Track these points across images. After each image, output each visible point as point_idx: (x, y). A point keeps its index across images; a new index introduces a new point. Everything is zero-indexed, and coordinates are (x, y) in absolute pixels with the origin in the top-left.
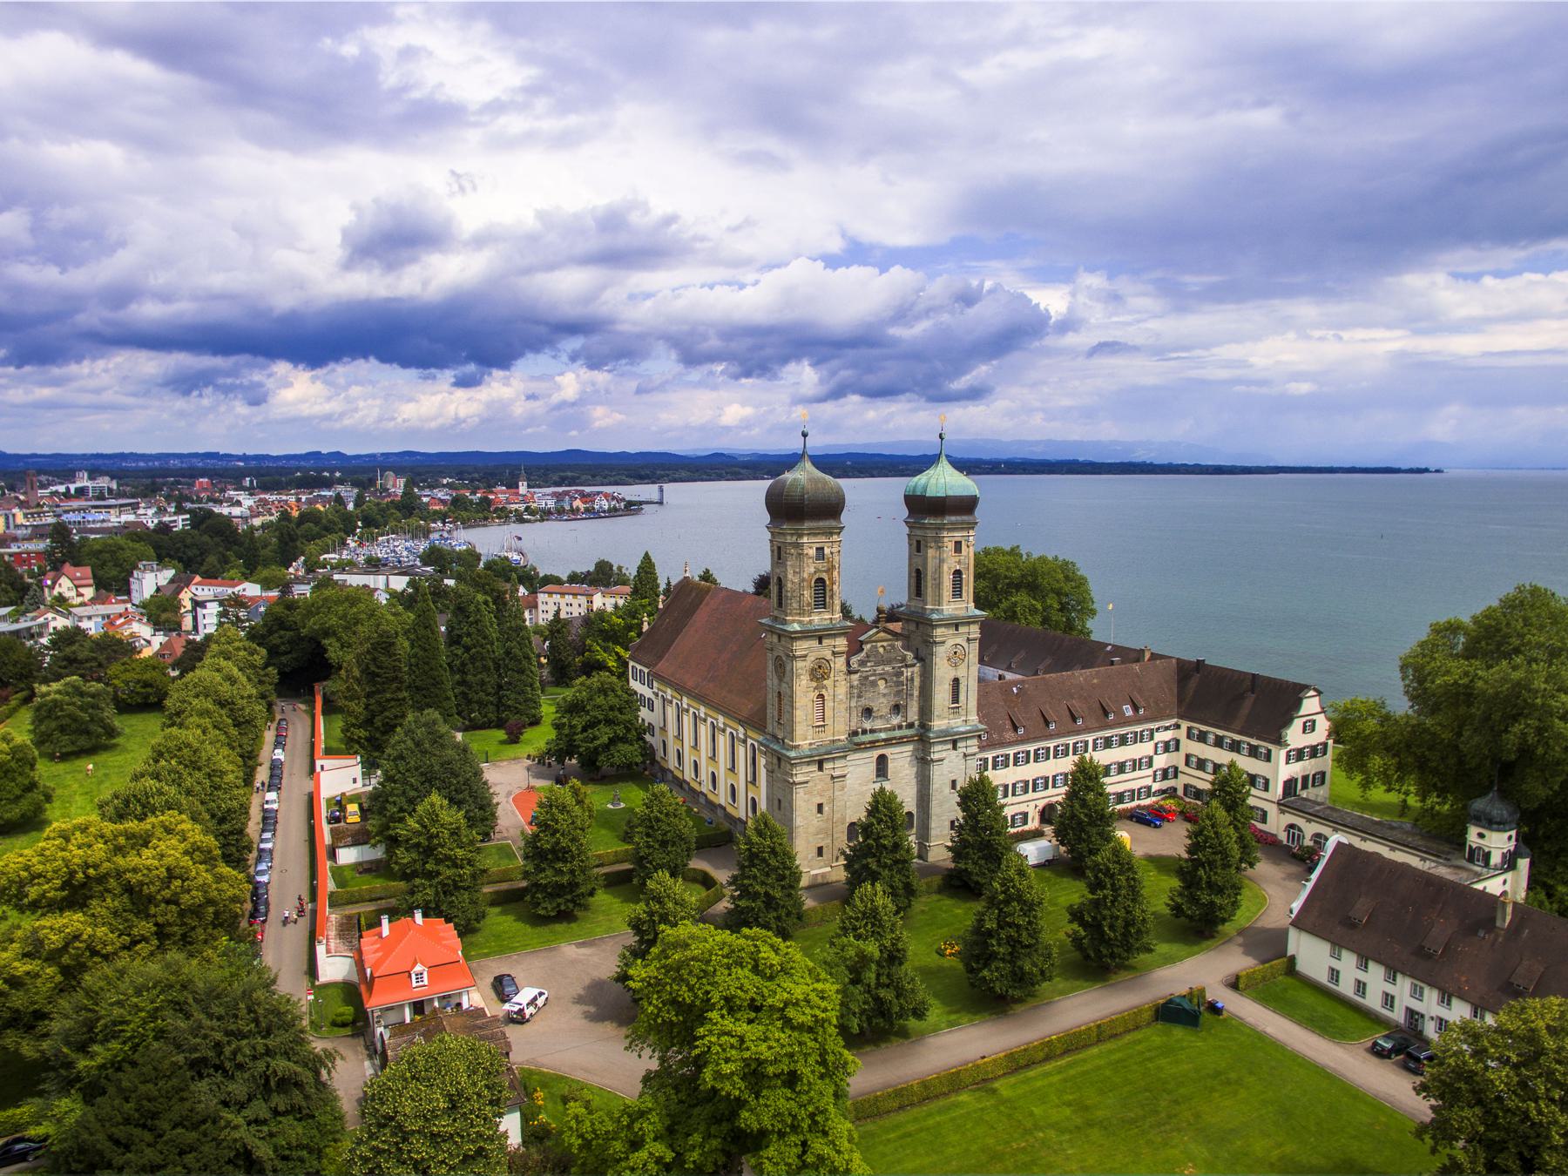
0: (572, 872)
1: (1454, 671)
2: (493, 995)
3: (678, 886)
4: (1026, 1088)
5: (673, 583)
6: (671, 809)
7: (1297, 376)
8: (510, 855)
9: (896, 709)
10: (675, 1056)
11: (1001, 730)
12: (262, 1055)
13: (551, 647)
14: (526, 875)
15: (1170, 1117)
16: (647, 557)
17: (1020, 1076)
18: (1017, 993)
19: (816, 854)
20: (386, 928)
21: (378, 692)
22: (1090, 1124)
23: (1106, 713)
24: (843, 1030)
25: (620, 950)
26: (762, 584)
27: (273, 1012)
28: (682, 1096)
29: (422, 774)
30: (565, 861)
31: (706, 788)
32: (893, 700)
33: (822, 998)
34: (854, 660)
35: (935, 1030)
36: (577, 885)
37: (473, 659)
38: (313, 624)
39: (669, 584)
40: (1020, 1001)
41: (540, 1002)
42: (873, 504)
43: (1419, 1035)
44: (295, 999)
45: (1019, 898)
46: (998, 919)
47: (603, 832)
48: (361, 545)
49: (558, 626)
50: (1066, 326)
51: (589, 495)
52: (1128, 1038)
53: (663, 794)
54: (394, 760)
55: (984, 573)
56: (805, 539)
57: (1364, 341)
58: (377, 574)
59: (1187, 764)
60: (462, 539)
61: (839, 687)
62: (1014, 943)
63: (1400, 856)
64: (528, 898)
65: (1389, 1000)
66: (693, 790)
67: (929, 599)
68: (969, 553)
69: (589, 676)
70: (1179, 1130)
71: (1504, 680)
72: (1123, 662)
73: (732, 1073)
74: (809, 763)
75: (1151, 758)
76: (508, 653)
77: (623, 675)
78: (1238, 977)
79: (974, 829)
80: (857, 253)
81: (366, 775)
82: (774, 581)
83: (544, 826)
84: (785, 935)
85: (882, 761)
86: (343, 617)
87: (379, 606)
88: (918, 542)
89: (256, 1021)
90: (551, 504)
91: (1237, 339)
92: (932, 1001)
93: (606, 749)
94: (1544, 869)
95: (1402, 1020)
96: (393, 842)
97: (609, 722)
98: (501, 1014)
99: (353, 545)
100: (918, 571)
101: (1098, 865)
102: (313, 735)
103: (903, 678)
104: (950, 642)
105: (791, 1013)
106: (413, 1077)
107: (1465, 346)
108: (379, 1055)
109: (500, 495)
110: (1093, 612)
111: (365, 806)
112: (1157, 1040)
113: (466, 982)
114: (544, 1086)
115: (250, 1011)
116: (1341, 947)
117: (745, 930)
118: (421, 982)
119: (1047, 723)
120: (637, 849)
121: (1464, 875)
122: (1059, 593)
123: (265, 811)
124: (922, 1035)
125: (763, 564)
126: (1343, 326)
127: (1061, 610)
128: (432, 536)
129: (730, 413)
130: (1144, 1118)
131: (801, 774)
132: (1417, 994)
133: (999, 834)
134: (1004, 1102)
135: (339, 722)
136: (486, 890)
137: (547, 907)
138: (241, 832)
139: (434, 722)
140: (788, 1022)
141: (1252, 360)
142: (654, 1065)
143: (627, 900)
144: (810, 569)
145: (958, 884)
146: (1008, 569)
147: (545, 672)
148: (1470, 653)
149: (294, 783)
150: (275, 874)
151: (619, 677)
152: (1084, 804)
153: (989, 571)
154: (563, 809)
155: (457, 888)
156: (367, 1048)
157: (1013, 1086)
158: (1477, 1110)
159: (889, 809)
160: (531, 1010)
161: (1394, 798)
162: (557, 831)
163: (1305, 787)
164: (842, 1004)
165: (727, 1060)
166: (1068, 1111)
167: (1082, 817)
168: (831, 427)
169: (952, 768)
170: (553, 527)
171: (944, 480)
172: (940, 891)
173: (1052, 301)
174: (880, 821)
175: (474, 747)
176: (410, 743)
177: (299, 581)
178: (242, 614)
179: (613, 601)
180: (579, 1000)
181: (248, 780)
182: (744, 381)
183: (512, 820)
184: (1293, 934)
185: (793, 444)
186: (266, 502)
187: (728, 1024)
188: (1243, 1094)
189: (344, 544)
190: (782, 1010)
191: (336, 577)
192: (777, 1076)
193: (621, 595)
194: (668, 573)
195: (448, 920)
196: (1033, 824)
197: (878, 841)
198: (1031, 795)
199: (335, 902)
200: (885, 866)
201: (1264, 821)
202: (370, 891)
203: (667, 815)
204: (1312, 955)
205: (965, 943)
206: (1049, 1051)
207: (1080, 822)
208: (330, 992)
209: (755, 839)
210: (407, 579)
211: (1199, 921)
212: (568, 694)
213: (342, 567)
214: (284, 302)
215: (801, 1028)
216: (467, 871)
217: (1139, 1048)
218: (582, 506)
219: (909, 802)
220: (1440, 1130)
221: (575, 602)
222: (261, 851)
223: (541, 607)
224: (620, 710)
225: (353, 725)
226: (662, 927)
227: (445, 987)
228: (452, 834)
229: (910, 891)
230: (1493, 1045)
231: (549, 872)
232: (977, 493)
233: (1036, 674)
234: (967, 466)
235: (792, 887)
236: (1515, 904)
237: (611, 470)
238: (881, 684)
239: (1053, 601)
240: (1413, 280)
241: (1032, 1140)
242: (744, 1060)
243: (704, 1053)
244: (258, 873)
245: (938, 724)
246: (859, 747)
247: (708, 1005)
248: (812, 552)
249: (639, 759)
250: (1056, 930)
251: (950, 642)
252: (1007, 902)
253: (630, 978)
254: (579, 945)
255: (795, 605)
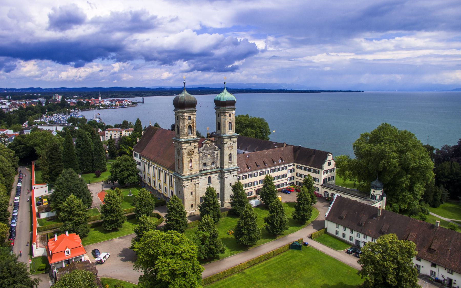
0: (116, 216)
1: (366, 147)
2: (92, 256)
3: (149, 219)
4: (254, 271)
5: (147, 127)
6: (147, 195)
7: (326, 65)
8: (97, 212)
9: (213, 163)
10: (149, 270)
11: (244, 168)
12: (12, 284)
13: (109, 147)
14: (102, 218)
15: (294, 276)
16: (138, 119)
17: (252, 268)
18: (250, 244)
19: (191, 206)
20: (56, 238)
21: (53, 163)
22: (272, 280)
23: (274, 162)
24: (199, 259)
25: (132, 239)
26: (173, 127)
27: (16, 269)
28: (151, 282)
29: (68, 188)
30: (114, 213)
31: (157, 188)
32: (212, 160)
33: (193, 250)
34: (200, 149)
35: (227, 256)
36: (118, 220)
37: (84, 152)
38: (31, 143)
39: (145, 127)
40: (251, 246)
41: (107, 257)
42: (205, 102)
43: (359, 247)
44: (25, 263)
45: (250, 217)
46: (243, 223)
47: (126, 203)
48: (47, 117)
49: (111, 141)
50: (263, 51)
51: (121, 101)
52: (282, 254)
53: (144, 191)
54: (59, 184)
55: (238, 122)
56: (185, 114)
57: (344, 56)
58: (53, 127)
59: (297, 176)
60: (80, 115)
61: (196, 157)
62: (249, 230)
63: (353, 199)
64: (103, 225)
65: (351, 238)
66: (154, 189)
67: (222, 131)
68: (233, 117)
69: (121, 156)
70: (296, 279)
71: (379, 149)
72: (278, 147)
73: (166, 274)
74: (188, 180)
75: (287, 174)
76: (95, 150)
77: (131, 156)
78: (311, 235)
79: (237, 197)
80: (204, 30)
81: (50, 190)
82: (176, 126)
83: (107, 203)
84: (182, 232)
85: (210, 178)
86: (42, 140)
87: (53, 136)
88: (219, 114)
89: (10, 273)
90: (109, 103)
91: (311, 55)
92: (226, 248)
93: (126, 179)
94: (389, 199)
95: (355, 243)
96: (59, 210)
97: (127, 170)
98: (95, 262)
99: (45, 117)
100: (219, 123)
101: (272, 206)
102: (31, 178)
103: (215, 154)
104: (228, 143)
105: (183, 255)
106: (65, 285)
107: (369, 57)
108: (54, 278)
109: (93, 100)
110: (270, 133)
111: (49, 199)
112: (290, 254)
113: (83, 253)
114: (109, 283)
115: (8, 269)
116: (339, 224)
117: (169, 231)
118: (68, 254)
119: (257, 166)
120: (137, 208)
121: (370, 202)
122: (260, 128)
123: (15, 203)
124: (223, 258)
125: (173, 121)
126: (338, 52)
127: (261, 133)
128: (71, 114)
129: (163, 76)
130: (287, 277)
131: (185, 183)
132: (358, 236)
133: (244, 198)
134: (247, 276)
135: (40, 173)
136: (89, 223)
137: (109, 227)
138: (6, 210)
139: (72, 172)
140: (182, 258)
141: (314, 61)
142: (143, 274)
143: (134, 224)
144: (187, 123)
145: (232, 213)
146: (245, 121)
147: (108, 155)
148: (370, 142)
149: (24, 192)
150: (18, 223)
151: (130, 156)
152: (268, 189)
153: (240, 122)
154: (113, 197)
155: (80, 223)
156: (50, 276)
157: (250, 271)
158: (373, 266)
159: (212, 193)
160: (105, 259)
161: (352, 182)
162: (111, 204)
163: (329, 180)
164: (199, 251)
165: (164, 271)
166: (265, 277)
167: (267, 192)
168: (193, 80)
169: (230, 180)
170: (109, 110)
171: (226, 96)
172: (228, 216)
173: (260, 44)
174: (209, 196)
175: (85, 179)
176: (64, 179)
177: (26, 129)
178: (6, 140)
179: (128, 133)
180: (120, 255)
181: (9, 193)
182: (163, 66)
183: (97, 201)
184: (326, 222)
185: (181, 85)
186: (14, 104)
187: (164, 259)
188: (313, 267)
189: (42, 117)
190: (181, 254)
191: (39, 127)
192: (180, 274)
193: (131, 131)
194: (145, 124)
195: (77, 234)
196: (254, 194)
197: (209, 202)
198: (253, 186)
199: (39, 231)
200: (211, 209)
201: (318, 191)
202: (51, 226)
203: (146, 197)
204: (331, 227)
205: (235, 230)
206: (260, 260)
207: (267, 194)
208: (37, 260)
209: (172, 203)
210: (62, 127)
211: (300, 221)
212: (114, 162)
213: (41, 124)
214: (24, 40)
215: (186, 259)
216: (83, 218)
217: (285, 257)
218: (119, 104)
219: (218, 190)
220: (363, 272)
221: (117, 133)
222: (13, 216)
223: (106, 135)
224: (131, 166)
225: (45, 174)
226: (144, 232)
227: (76, 255)
228: (78, 207)
229: (219, 216)
230: (376, 248)
231: (109, 217)
232: (235, 100)
233: (254, 151)
234: (232, 91)
235: (184, 217)
236: (382, 209)
237: (128, 93)
238: (209, 156)
239: (258, 130)
240: (357, 40)
241: (255, 286)
242: (169, 270)
243: (157, 269)
244: (12, 223)
245: (226, 167)
246: (203, 175)
247: (158, 254)
248: (187, 118)
249: (137, 181)
250: (261, 225)
251: (228, 143)
252: (247, 218)
253: (134, 248)
254: (119, 238)
255: (183, 133)
